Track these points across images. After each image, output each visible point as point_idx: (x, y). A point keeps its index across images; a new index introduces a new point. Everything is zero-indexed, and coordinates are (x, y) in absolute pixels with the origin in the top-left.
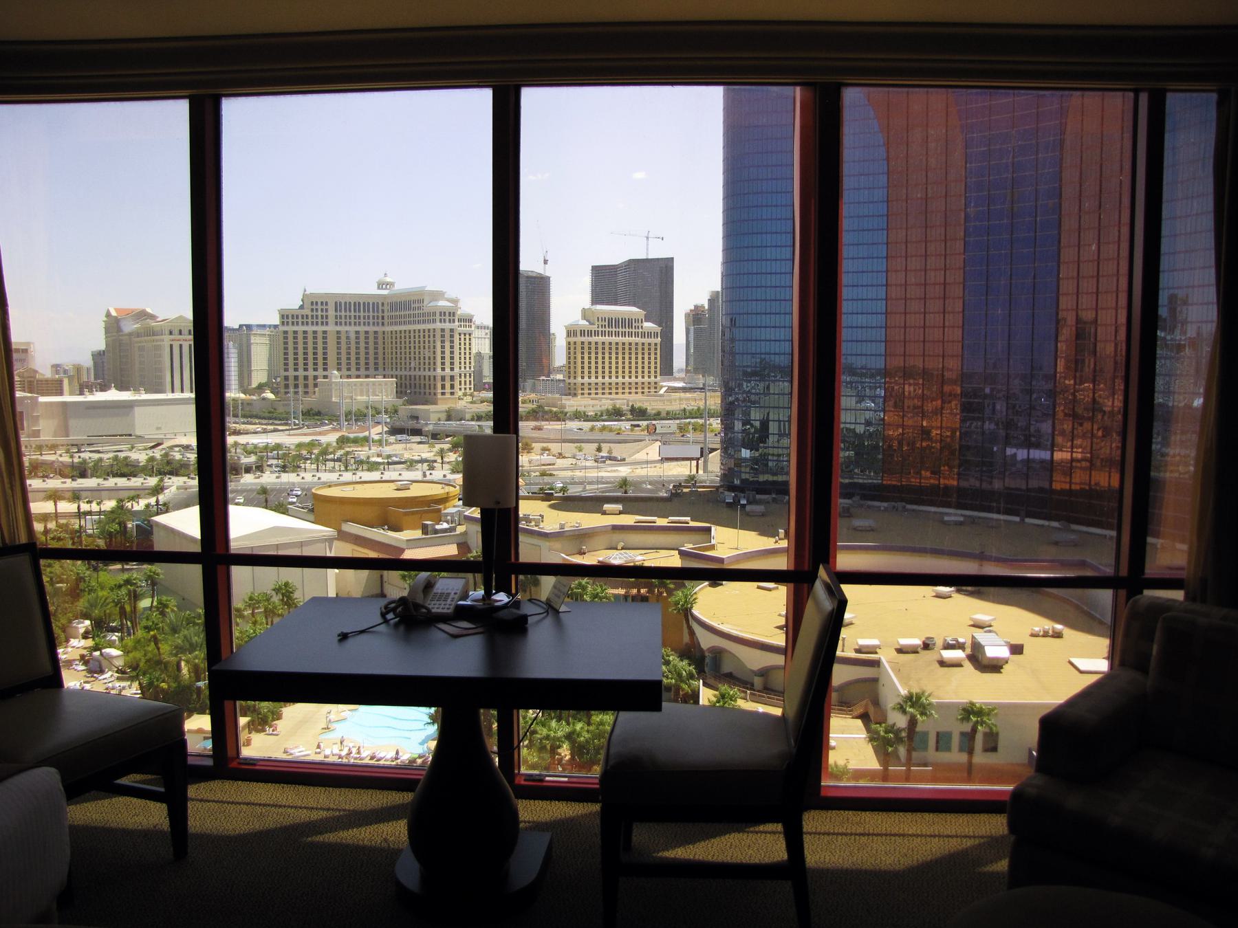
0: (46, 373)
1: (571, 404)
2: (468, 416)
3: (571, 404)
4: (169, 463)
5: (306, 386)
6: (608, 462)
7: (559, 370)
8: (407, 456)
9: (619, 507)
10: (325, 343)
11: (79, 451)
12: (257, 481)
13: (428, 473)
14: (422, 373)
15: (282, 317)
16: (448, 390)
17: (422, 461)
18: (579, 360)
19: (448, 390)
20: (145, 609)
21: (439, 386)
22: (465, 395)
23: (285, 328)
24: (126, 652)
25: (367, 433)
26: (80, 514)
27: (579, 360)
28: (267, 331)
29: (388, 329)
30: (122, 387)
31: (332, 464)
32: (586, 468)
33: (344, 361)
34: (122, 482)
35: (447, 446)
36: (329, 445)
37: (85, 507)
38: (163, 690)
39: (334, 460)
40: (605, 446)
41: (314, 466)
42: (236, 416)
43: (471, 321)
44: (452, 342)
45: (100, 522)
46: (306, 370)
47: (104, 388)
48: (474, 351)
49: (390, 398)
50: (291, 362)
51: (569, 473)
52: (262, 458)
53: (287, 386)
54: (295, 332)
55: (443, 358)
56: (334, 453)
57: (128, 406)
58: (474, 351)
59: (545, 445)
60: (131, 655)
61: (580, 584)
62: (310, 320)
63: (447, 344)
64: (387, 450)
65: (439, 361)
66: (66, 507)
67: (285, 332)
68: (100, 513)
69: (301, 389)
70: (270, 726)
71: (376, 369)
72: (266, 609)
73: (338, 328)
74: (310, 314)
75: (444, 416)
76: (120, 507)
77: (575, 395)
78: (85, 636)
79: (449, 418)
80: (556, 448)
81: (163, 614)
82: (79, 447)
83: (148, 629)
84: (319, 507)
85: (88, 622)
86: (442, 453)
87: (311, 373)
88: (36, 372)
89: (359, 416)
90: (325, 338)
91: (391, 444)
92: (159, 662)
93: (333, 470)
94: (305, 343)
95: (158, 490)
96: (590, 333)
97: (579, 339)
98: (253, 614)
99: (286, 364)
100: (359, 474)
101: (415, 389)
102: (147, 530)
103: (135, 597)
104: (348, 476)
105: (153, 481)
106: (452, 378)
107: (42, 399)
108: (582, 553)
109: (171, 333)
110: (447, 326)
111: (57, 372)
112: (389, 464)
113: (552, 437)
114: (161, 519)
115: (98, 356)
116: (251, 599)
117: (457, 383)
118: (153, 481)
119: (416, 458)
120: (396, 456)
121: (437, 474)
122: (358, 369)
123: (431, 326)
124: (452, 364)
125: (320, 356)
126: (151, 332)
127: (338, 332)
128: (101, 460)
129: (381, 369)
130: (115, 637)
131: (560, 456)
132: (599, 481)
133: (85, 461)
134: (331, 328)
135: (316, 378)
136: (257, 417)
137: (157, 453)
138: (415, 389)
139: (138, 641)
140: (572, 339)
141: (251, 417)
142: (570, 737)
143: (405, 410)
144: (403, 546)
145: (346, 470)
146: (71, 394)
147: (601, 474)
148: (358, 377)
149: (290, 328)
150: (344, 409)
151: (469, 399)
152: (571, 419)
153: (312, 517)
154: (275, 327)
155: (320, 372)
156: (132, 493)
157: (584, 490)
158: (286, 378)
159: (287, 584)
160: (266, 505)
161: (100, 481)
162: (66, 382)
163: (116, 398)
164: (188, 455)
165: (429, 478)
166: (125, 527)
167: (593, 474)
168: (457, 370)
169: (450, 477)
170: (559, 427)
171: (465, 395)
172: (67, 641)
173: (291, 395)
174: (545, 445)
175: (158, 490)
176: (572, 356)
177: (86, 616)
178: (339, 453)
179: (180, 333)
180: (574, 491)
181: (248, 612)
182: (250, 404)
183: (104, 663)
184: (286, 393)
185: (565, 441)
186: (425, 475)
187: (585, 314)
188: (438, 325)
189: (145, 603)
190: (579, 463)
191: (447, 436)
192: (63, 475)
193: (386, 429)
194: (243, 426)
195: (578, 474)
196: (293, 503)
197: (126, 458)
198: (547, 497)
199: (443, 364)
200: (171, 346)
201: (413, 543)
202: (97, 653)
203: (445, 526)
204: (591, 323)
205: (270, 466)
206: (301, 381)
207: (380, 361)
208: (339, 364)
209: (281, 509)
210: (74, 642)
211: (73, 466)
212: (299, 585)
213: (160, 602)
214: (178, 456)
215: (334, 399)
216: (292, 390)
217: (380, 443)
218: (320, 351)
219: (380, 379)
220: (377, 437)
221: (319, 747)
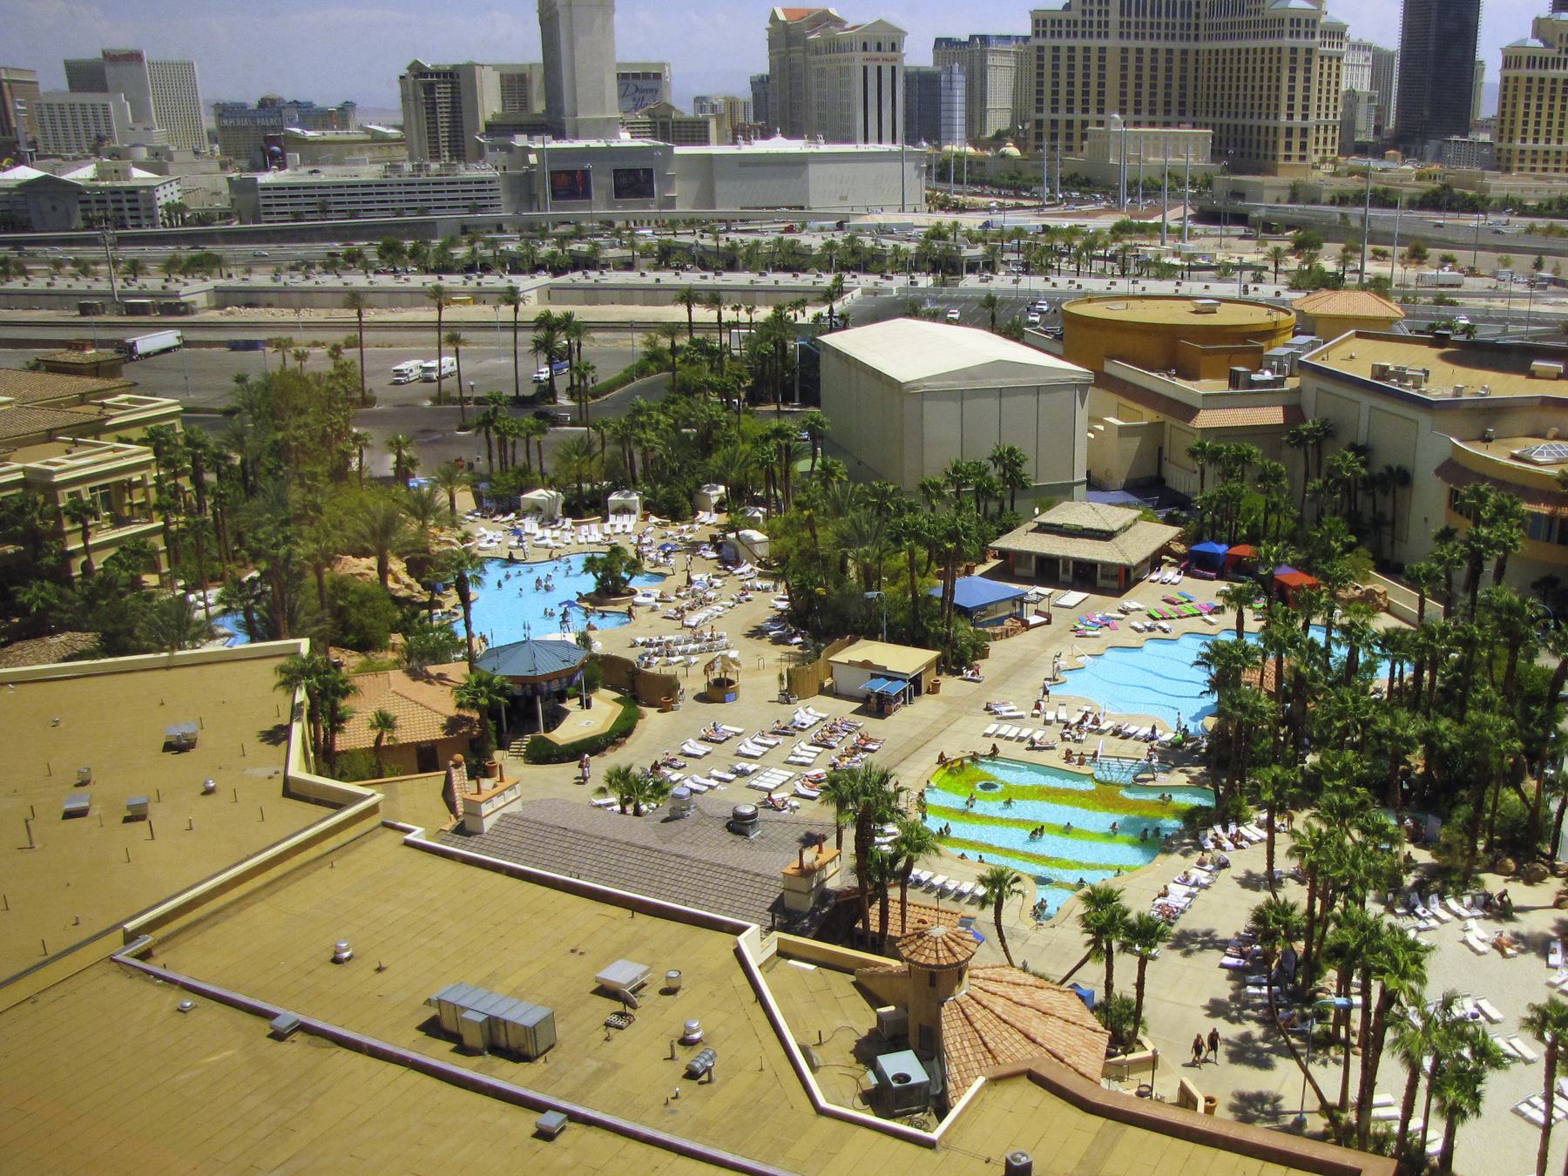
0: (687, 110)
1: (1500, 185)
2: (1325, 197)
3: (1500, 185)
4: (854, 252)
5: (1069, 137)
6: (1552, 288)
7: (1484, 126)
8: (1220, 257)
9: (1559, 367)
10: (1102, 67)
11: (728, 230)
12: (984, 285)
13: (1251, 287)
14: (1255, 122)
15: (1036, 23)
16: (1296, 152)
17: (1242, 267)
18: (1521, 109)
19: (1296, 152)
20: (803, 474)
21: (1282, 142)
22: (1323, 160)
23: (1041, 42)
24: (772, 535)
25: (1158, 219)
26: (721, 326)
27: (1521, 109)
28: (1012, 47)
29: (1204, 45)
30: (791, 133)
31: (1100, 264)
32: (1510, 295)
33: (1130, 98)
34: (785, 279)
35: (1285, 245)
36: (1098, 233)
37: (728, 315)
38: (820, 597)
39: (1104, 258)
40: (1548, 261)
41: (1073, 267)
42: (959, 181)
43: (1342, 35)
44: (1308, 70)
45: (748, 338)
46: (1070, 110)
47: (766, 134)
48: (1343, 88)
49: (1201, 162)
50: (1047, 96)
51: (1483, 303)
52: (994, 249)
53: (1039, 137)
54: (1087, 49)
55: (1291, 98)
56: (1105, 247)
57: (800, 161)
58: (1343, 88)
59: (1446, 252)
60: (779, 542)
61: (1476, 490)
62: (1079, 29)
63: (1300, 75)
64: (1191, 246)
65: (1284, 102)
66: (702, 314)
67: (1040, 49)
68: (751, 325)
69: (1060, 142)
70: (969, 668)
71: (1182, 113)
72: (978, 487)
73: (1125, 43)
74: (1080, 18)
75: (1286, 194)
76: (779, 320)
77: (1508, 170)
78: (719, 509)
79: (1294, 198)
80: (1464, 257)
81: (826, 483)
82: (729, 223)
83: (801, 506)
84: (1071, 333)
85: (722, 489)
86: (1277, 256)
87: (1078, 116)
88: (671, 108)
89: (1150, 190)
90: (1102, 59)
91: (1197, 236)
92: (815, 557)
93: (1101, 274)
94: (1139, 68)
95: (830, 296)
96: (1544, 63)
97: (1524, 72)
98: (958, 493)
99: (1039, 101)
100: (1142, 283)
101: (1245, 149)
102: (813, 356)
103: (790, 455)
104: (1123, 286)
105: (827, 280)
106: (1304, 132)
107: (678, 150)
108: (1486, 439)
109: (865, 47)
110: (1302, 43)
111: (702, 109)
112: (1190, 268)
113: (1461, 239)
114: (827, 339)
115: (759, 84)
116: (956, 470)
117: (1311, 141)
118: (827, 280)
119: (1235, 261)
120: (1203, 256)
121: (1266, 291)
122: (1152, 112)
123: (1273, 43)
124: (1305, 108)
125: (1094, 89)
126: (835, 46)
127: (1125, 50)
128: (757, 244)
129: (1189, 114)
130: (758, 513)
131: (1472, 272)
132: (1532, 318)
133: (734, 246)
134: (1113, 43)
135: (1085, 124)
136: (992, 184)
137: (839, 238)
138: (1245, 149)
139: (790, 522)
140: (1512, 73)
141: (982, 183)
142: (1427, 738)
143: (1224, 181)
144: (1198, 404)
145: (1123, 275)
146: (721, 142)
147: (1534, 308)
148: (1152, 124)
149: (1048, 42)
150: (1126, 177)
151: (1329, 168)
152: (1496, 211)
153: (1059, 348)
154: (1026, 39)
155: (1093, 115)
156: (800, 296)
157: (1505, 332)
158: (1039, 124)
159: (1011, 451)
160: (993, 326)
161: (754, 276)
162: (713, 125)
163: (781, 150)
164: (884, 241)
165: (1252, 295)
166: (784, 347)
167: (1522, 306)
168: (1313, 119)
169: (1287, 295)
170: (1473, 223)
171: (1323, 160)
172: (695, 514)
173: (1044, 151)
174: (1446, 252)
175: (830, 296)
176: (1509, 101)
177: (719, 480)
178: (1114, 248)
179: (879, 46)
180: (1485, 333)
181: (949, 491)
182: (981, 163)
183: (742, 551)
184: (1037, 147)
185: (1483, 248)
186: (1246, 291)
187: (1539, 27)
188: (1287, 42)
189: (803, 465)
190: (1502, 286)
191: (1289, 228)
192: (704, 267)
193: (1190, 212)
194: (969, 199)
195: (1498, 304)
196: (1034, 324)
197: (793, 242)
198: (1439, 341)
199: (1291, 107)
200: (865, 69)
201: (1213, 401)
202: (732, 536)
203: (1268, 375)
204: (1548, 45)
205: (1006, 263)
206: (1062, 130)
207: (1189, 100)
208: (1123, 103)
209: (1014, 333)
210: (703, 516)
211: (717, 253)
212: (1031, 456)
213: (824, 466)
214: (868, 242)
215: (1111, 161)
216: (1046, 143)
217: (1179, 234)
218: (1094, 81)
219: (1187, 130)
220: (1175, 225)
221: (1038, 706)
